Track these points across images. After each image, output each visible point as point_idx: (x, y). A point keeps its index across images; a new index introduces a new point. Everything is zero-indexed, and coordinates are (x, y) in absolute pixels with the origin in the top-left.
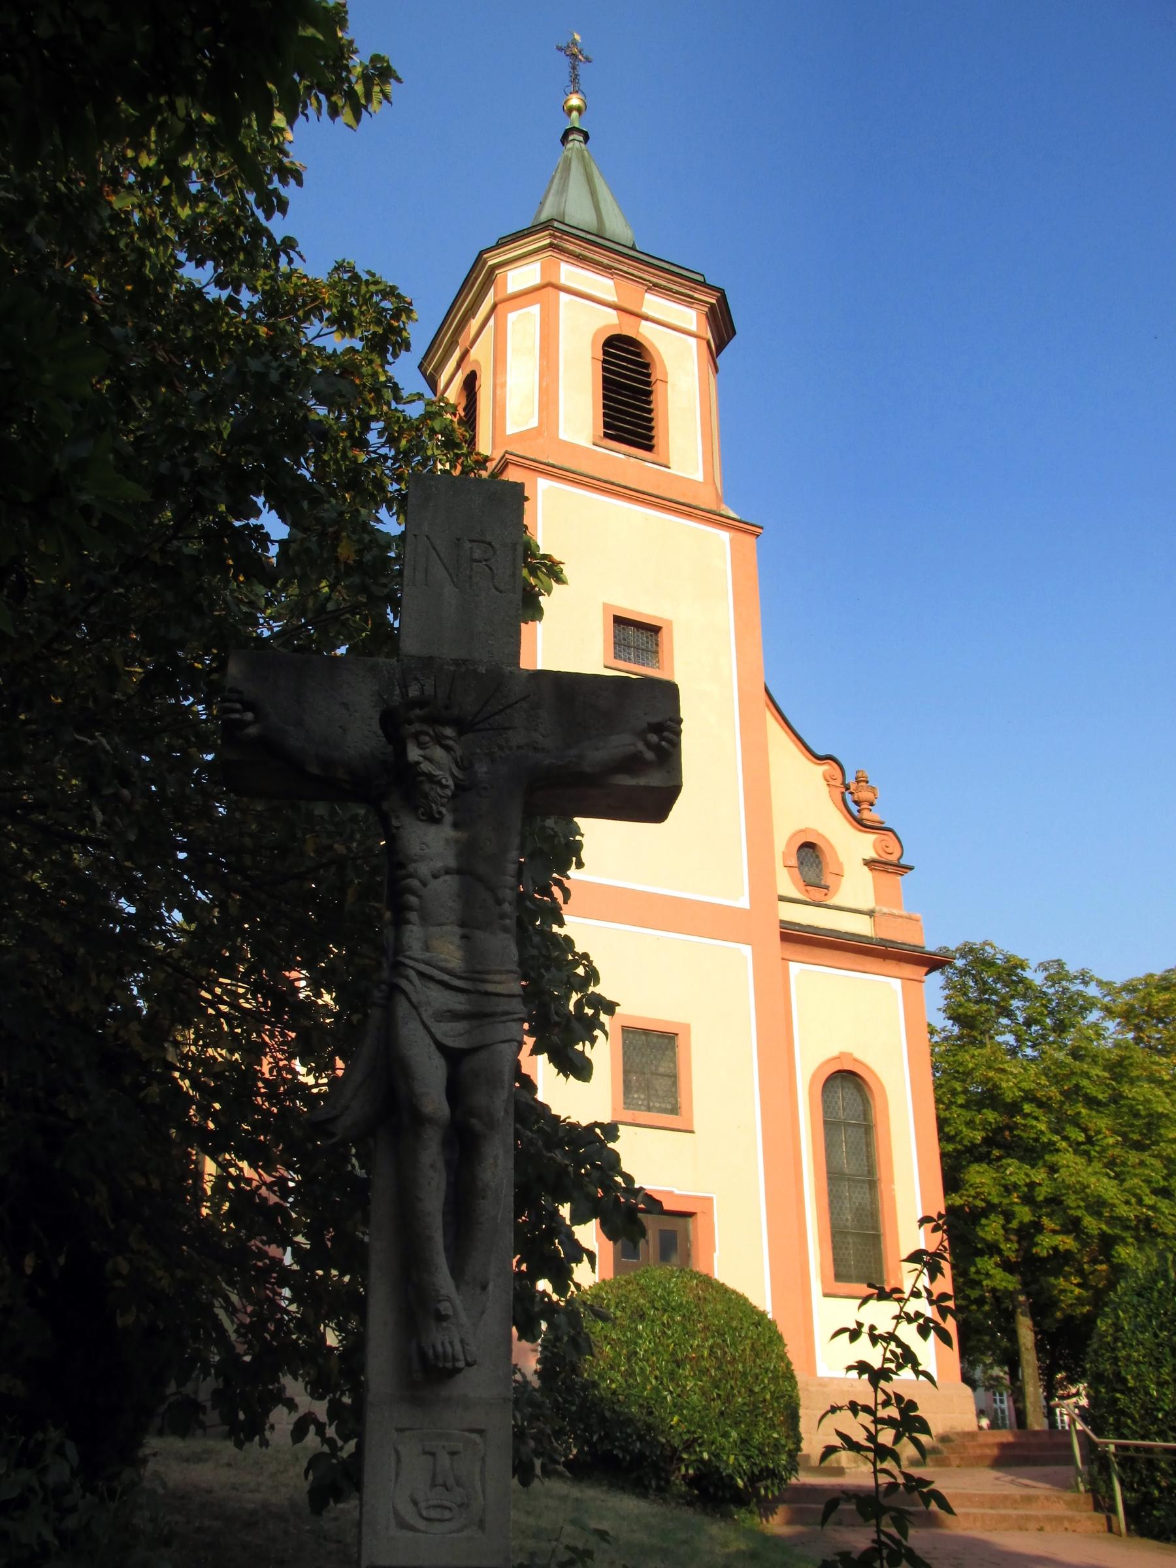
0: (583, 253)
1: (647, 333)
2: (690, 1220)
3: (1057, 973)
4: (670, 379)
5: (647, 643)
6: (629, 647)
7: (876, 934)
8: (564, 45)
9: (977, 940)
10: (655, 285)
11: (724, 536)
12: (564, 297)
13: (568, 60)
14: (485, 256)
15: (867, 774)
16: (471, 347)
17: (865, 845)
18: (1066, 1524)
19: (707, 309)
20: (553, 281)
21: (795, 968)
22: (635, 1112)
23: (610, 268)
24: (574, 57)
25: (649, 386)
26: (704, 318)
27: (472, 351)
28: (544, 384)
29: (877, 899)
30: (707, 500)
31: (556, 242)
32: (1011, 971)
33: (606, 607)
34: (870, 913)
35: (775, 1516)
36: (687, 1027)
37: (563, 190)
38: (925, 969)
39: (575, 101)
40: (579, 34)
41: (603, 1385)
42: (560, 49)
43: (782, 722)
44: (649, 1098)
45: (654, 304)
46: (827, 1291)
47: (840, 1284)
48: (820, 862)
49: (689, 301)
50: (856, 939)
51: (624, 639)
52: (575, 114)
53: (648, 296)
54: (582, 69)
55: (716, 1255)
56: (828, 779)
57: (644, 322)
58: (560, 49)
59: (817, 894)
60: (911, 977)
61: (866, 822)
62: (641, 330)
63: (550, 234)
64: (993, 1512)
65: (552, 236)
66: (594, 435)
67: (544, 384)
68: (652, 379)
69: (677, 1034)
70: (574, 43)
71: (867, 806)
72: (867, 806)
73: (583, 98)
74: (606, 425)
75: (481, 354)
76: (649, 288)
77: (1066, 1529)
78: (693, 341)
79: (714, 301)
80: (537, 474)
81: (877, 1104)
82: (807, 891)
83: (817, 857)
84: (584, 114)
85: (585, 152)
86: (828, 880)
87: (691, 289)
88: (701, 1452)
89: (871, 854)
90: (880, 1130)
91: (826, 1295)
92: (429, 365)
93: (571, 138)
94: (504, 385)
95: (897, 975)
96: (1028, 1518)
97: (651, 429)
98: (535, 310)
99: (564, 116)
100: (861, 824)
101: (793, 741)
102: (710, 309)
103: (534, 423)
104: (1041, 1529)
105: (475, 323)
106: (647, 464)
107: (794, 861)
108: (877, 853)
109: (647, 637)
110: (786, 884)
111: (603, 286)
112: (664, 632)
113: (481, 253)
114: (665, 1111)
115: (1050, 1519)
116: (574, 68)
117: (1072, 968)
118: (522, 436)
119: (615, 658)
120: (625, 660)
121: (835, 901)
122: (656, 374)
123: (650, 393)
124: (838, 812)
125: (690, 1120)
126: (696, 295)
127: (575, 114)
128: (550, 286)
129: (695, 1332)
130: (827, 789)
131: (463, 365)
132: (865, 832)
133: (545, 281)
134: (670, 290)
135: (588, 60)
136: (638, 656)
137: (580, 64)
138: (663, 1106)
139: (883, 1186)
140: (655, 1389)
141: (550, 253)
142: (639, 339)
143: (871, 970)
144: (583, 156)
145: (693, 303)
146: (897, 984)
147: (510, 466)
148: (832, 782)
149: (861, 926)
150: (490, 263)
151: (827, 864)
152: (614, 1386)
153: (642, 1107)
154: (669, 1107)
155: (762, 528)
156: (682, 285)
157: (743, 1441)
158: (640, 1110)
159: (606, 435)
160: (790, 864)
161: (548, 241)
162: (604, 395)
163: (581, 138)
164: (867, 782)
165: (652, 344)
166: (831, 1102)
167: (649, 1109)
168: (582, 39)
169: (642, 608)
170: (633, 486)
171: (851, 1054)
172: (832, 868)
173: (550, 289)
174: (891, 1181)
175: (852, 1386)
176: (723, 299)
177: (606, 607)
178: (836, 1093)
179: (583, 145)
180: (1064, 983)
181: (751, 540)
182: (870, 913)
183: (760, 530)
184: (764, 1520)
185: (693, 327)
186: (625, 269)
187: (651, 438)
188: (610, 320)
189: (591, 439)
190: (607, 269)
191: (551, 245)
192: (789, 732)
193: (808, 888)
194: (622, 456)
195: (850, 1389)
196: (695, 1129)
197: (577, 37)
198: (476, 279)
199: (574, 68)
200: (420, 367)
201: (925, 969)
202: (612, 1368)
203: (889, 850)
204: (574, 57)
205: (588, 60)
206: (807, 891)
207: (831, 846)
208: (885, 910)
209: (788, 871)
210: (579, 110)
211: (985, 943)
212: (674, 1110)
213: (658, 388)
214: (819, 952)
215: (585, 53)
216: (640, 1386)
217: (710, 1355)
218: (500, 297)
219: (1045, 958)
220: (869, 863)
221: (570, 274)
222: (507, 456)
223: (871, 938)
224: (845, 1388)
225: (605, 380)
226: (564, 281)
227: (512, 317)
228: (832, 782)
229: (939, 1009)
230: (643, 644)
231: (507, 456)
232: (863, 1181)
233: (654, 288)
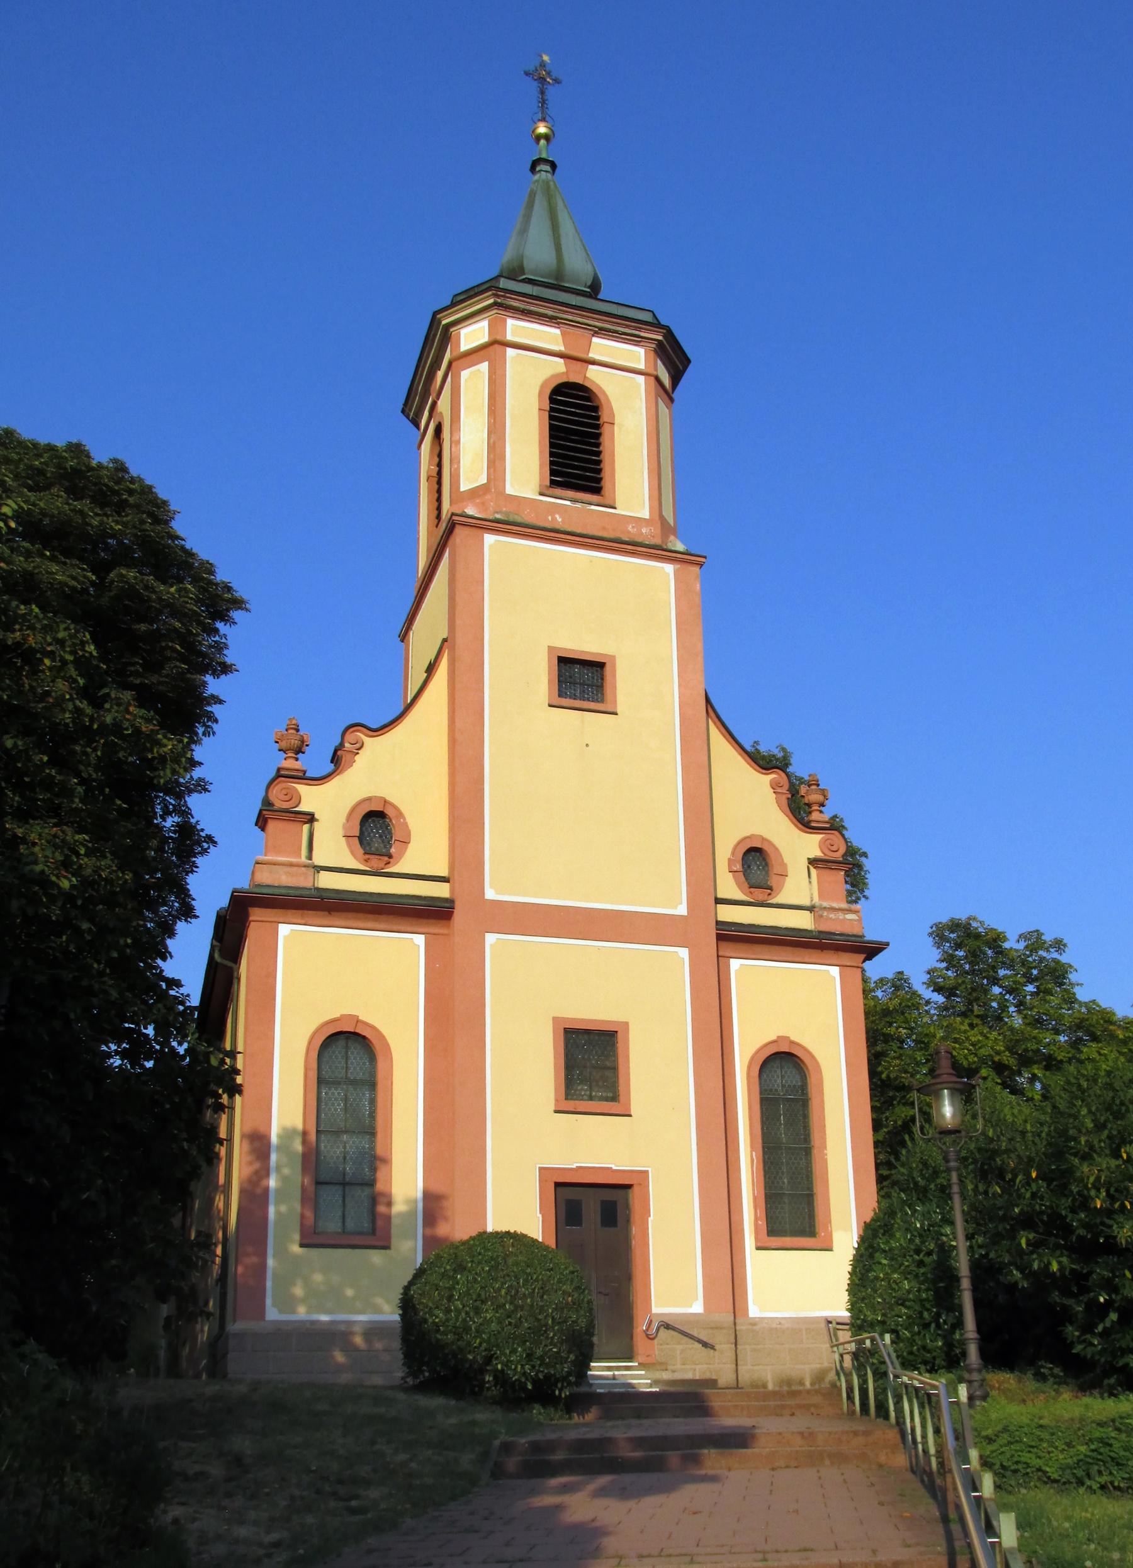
0: (528, 307)
1: (595, 376)
2: (630, 1190)
3: (1035, 941)
4: (617, 421)
5: (593, 678)
6: (575, 683)
7: (815, 928)
8: (531, 68)
9: (962, 915)
10: (601, 329)
11: (669, 568)
12: (510, 352)
13: (535, 84)
14: (438, 316)
15: (819, 777)
16: (438, 399)
17: (811, 845)
18: (812, 1409)
19: (654, 346)
20: (499, 338)
21: (735, 964)
22: (576, 1102)
23: (556, 318)
24: (541, 78)
25: (598, 429)
26: (652, 354)
27: (439, 403)
28: (492, 441)
29: (821, 895)
30: (648, 534)
31: (499, 301)
32: (995, 940)
33: (551, 649)
34: (811, 909)
35: (589, 1414)
36: (626, 1025)
37: (524, 231)
38: (863, 956)
39: (542, 129)
40: (546, 54)
41: (430, 1320)
42: (527, 74)
43: (728, 736)
44: (591, 1089)
45: (602, 348)
46: (759, 1244)
47: (772, 1238)
48: (767, 864)
49: (636, 340)
50: (791, 933)
51: (571, 677)
52: (543, 142)
53: (595, 340)
54: (552, 92)
55: (650, 1219)
56: (774, 786)
57: (590, 367)
58: (527, 74)
59: (760, 895)
60: (848, 964)
61: (813, 824)
62: (588, 375)
63: (493, 294)
64: (756, 1403)
65: (496, 295)
66: (540, 485)
67: (492, 441)
68: (601, 422)
69: (616, 1032)
70: (543, 65)
71: (817, 808)
72: (817, 808)
73: (549, 126)
74: (553, 473)
75: (444, 405)
76: (596, 332)
77: (812, 1414)
78: (641, 379)
79: (660, 338)
80: (484, 530)
81: (812, 1080)
82: (751, 892)
83: (764, 859)
84: (553, 142)
85: (552, 183)
86: (773, 881)
87: (636, 329)
88: (497, 1364)
89: (817, 853)
90: (814, 1103)
91: (758, 1248)
92: (410, 410)
93: (538, 169)
94: (458, 442)
95: (835, 963)
96: (783, 1407)
97: (599, 471)
98: (484, 367)
99: (534, 143)
100: (806, 826)
101: (740, 754)
102: (657, 345)
103: (483, 480)
104: (793, 1414)
105: (440, 374)
106: (593, 507)
107: (738, 867)
108: (823, 853)
109: (593, 673)
110: (728, 887)
111: (549, 336)
112: (608, 668)
113: (435, 314)
114: (607, 1099)
115: (800, 1406)
116: (542, 93)
117: (1048, 937)
118: (474, 493)
119: (559, 696)
120: (570, 698)
121: (779, 899)
122: (605, 417)
123: (598, 436)
124: (787, 818)
125: (628, 1104)
126: (642, 334)
127: (543, 142)
128: (497, 344)
129: (497, 1277)
130: (774, 795)
131: (434, 414)
132: (811, 833)
133: (493, 338)
134: (616, 332)
135: (557, 81)
136: (584, 691)
137: (549, 87)
138: (604, 1094)
139: (815, 1152)
140: (464, 1320)
141: (495, 311)
142: (587, 384)
143: (811, 961)
144: (548, 187)
145: (640, 342)
146: (835, 971)
147: (457, 526)
148: (779, 790)
149: (802, 921)
150: (444, 322)
151: (772, 866)
152: (437, 1320)
153: (585, 1097)
154: (610, 1095)
155: (705, 557)
156: (627, 326)
157: (528, 1355)
158: (582, 1100)
159: (553, 482)
160: (735, 869)
161: (491, 301)
162: (551, 443)
163: (548, 168)
164: (818, 785)
165: (600, 388)
166: (770, 1080)
167: (591, 1098)
168: (550, 60)
169: (586, 645)
170: (579, 531)
171: (789, 1037)
172: (776, 869)
173: (496, 346)
174: (824, 1146)
175: (780, 1324)
176: (669, 334)
177: (551, 649)
178: (776, 1072)
179: (549, 175)
180: (1041, 953)
181: (695, 569)
182: (811, 909)
183: (703, 560)
184: (581, 1417)
185: (641, 366)
186: (570, 317)
187: (599, 480)
188: (556, 368)
189: (537, 489)
190: (551, 320)
191: (495, 304)
192: (736, 746)
193: (752, 890)
194: (568, 503)
195: (779, 1326)
196: (632, 1114)
197: (546, 58)
198: (435, 336)
199: (542, 93)
200: (403, 411)
201: (863, 956)
202: (437, 1307)
203: (834, 848)
204: (541, 78)
205: (557, 81)
206: (751, 892)
207: (776, 849)
208: (825, 904)
209: (734, 876)
210: (547, 137)
211: (969, 919)
212: (615, 1098)
213: (605, 430)
214: (758, 948)
215: (554, 75)
216: (454, 1319)
217: (507, 1294)
218: (455, 354)
219: (1024, 929)
220: (813, 862)
221: (516, 328)
222: (455, 518)
223: (811, 931)
224: (774, 1326)
225: (552, 428)
226: (510, 337)
227: (465, 374)
228: (779, 790)
229: (923, 983)
230: (588, 680)
231: (455, 518)
232: (801, 1149)
233: (600, 332)
